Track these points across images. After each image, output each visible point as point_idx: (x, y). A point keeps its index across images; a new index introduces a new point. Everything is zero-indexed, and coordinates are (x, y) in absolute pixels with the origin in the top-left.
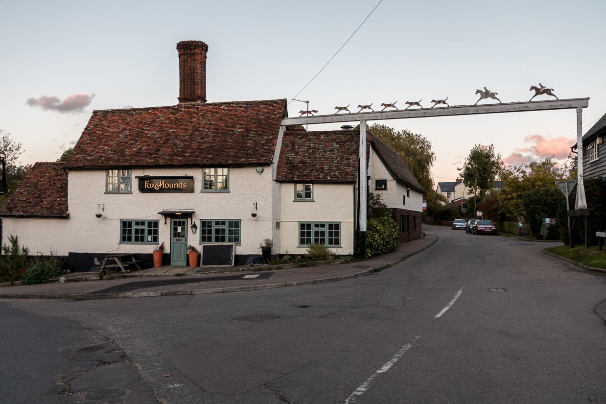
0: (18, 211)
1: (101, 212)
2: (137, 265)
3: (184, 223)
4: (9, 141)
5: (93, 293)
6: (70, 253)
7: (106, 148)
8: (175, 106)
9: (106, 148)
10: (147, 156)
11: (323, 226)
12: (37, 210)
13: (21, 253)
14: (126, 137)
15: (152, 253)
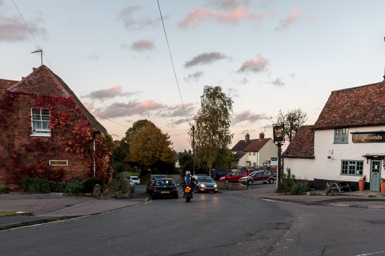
0: (291, 154)
1: (331, 155)
2: (349, 188)
3: (379, 163)
4: (301, 112)
5: (315, 202)
6: (314, 179)
7: (336, 115)
8: (381, 83)
9: (336, 115)
10: (358, 119)
11: (354, 163)
12: (299, 154)
13: (291, 177)
14: (348, 107)
15: (358, 181)
